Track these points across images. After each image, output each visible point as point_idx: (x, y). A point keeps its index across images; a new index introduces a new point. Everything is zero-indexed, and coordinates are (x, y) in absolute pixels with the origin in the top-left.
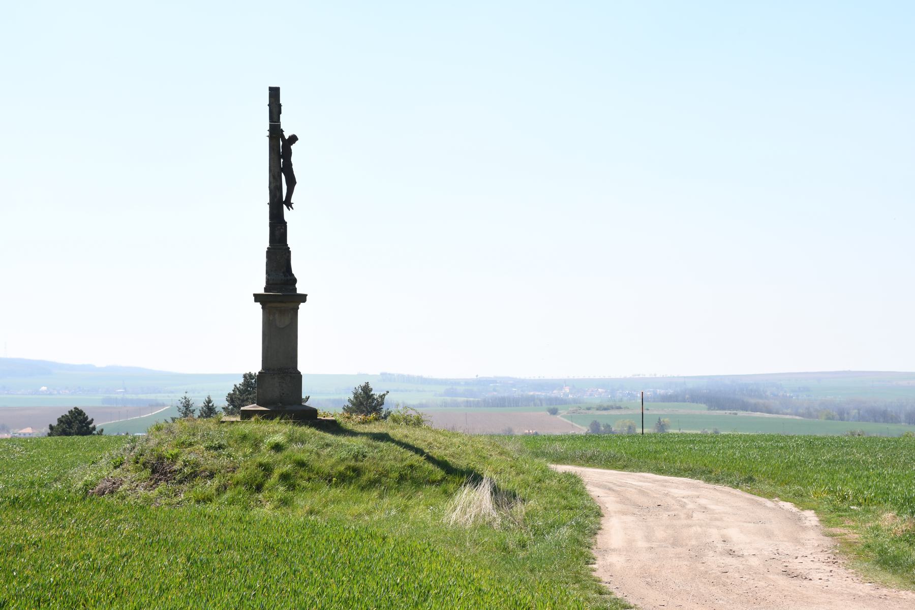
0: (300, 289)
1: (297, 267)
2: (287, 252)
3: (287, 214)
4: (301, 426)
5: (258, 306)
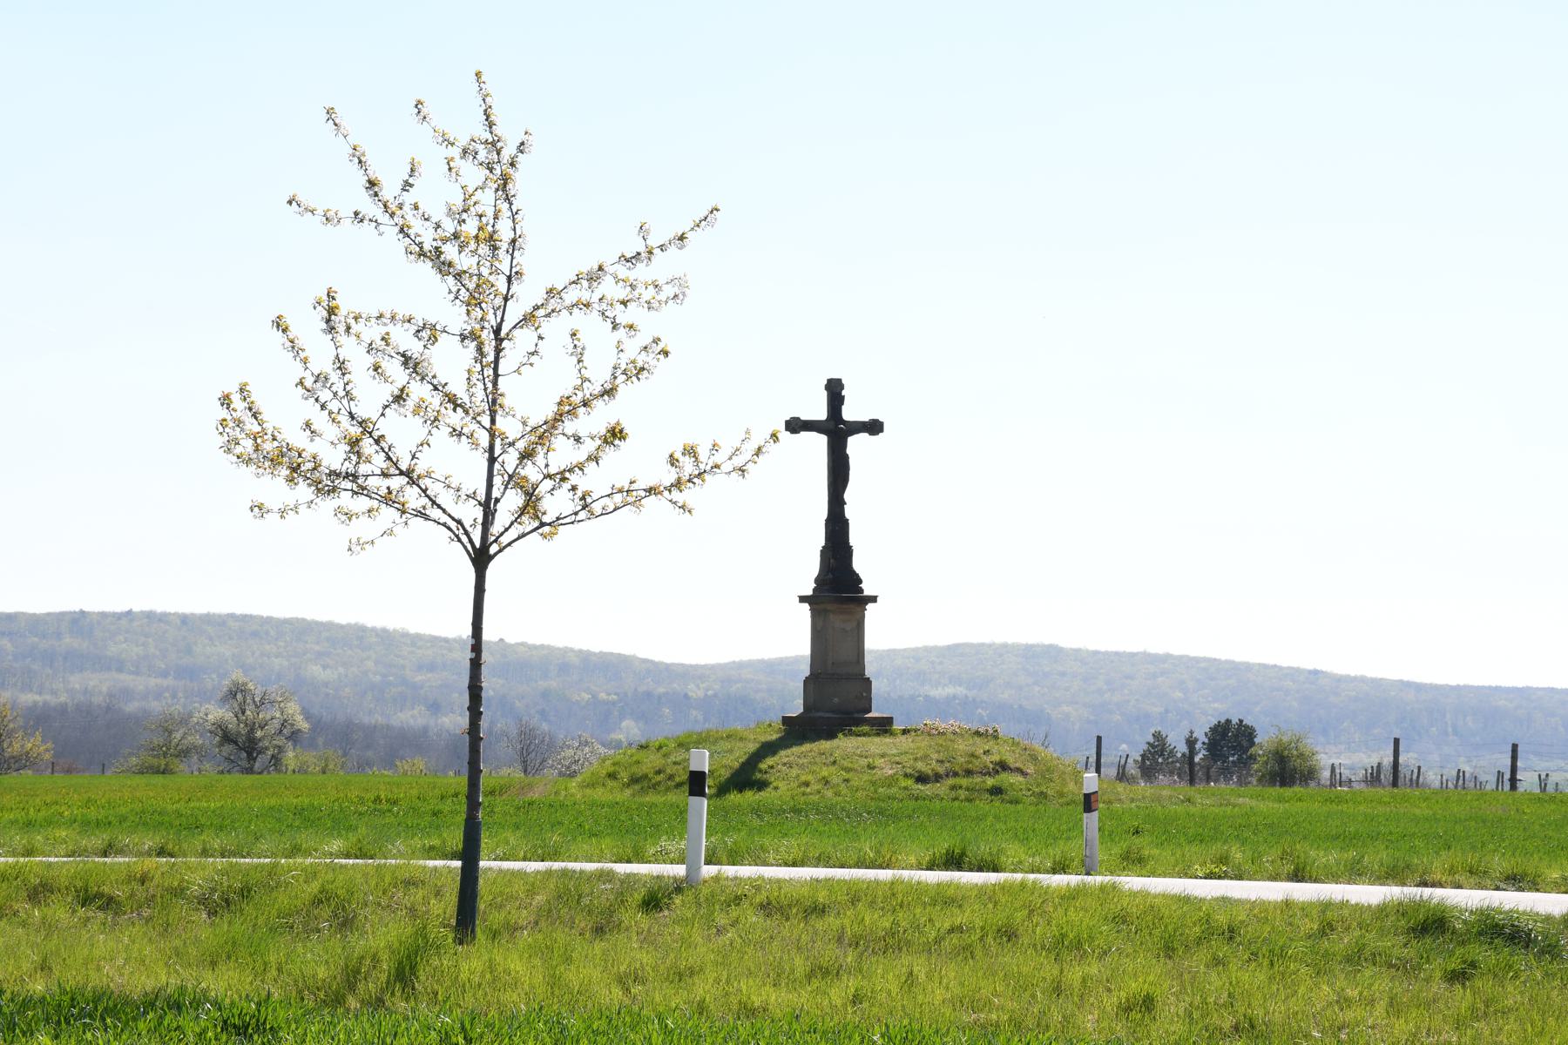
0: (868, 589)
1: (860, 563)
4: (425, 730)
5: (806, 606)
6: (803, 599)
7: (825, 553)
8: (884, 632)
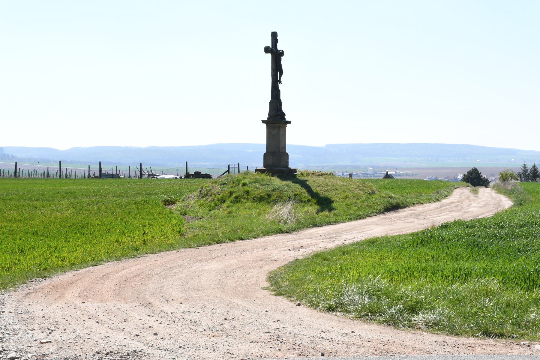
0: (287, 118)
1: (285, 108)
2: (280, 103)
3: (280, 87)
4: (272, 176)
5: (265, 125)
6: (263, 122)
7: (271, 103)
8: (293, 137)
